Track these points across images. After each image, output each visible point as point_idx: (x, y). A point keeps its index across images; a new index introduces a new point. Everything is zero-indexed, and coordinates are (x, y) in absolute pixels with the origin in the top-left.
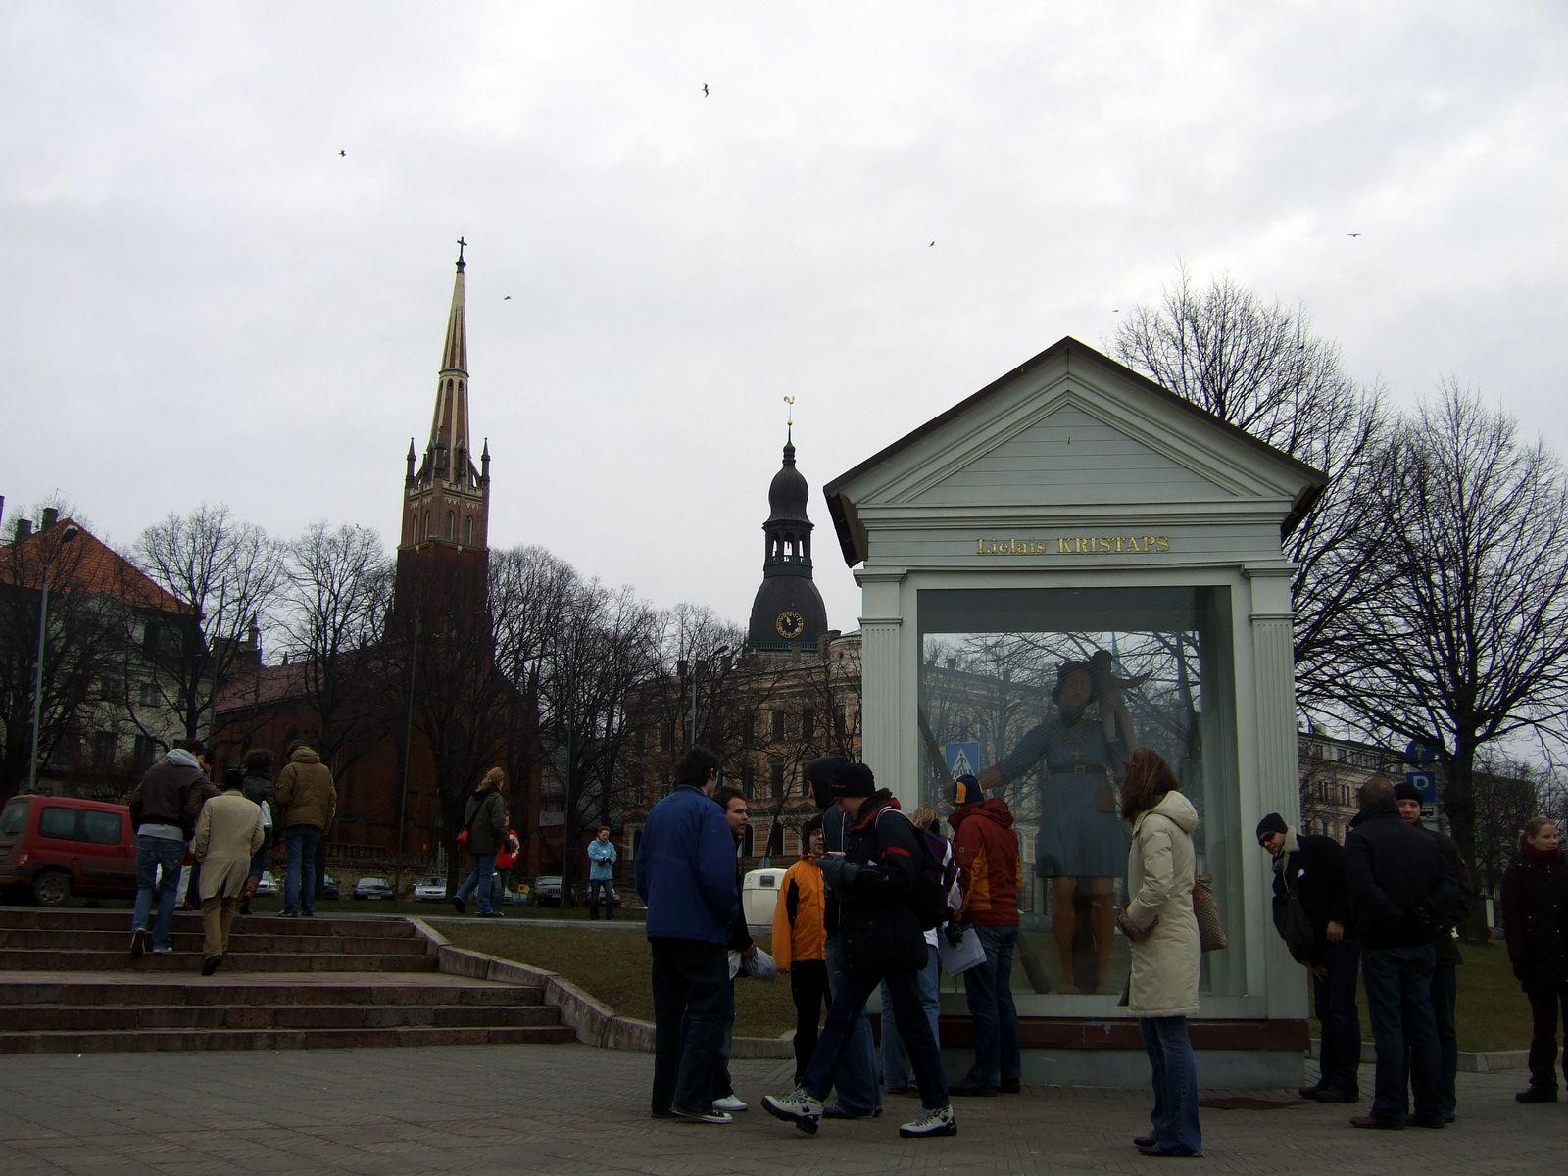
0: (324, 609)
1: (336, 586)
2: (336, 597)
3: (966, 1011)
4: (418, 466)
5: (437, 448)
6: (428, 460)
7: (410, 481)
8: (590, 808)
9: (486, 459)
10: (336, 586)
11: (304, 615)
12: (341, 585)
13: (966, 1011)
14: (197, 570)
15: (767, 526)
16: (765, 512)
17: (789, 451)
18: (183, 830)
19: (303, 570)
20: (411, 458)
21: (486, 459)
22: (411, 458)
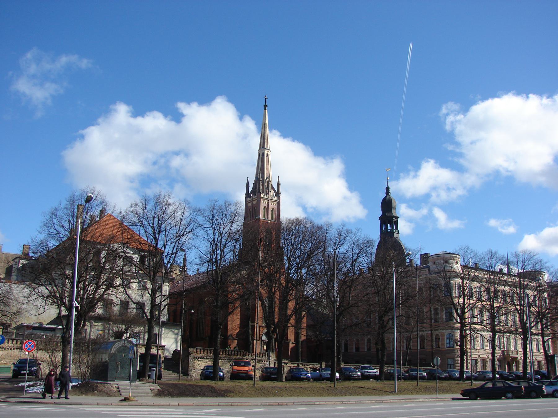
0: (216, 240)
1: (222, 229)
2: (221, 234)
3: (191, 350)
4: (251, 189)
5: (257, 180)
6: (255, 186)
7: (248, 195)
8: (462, 301)
9: (278, 184)
10: (222, 229)
11: (208, 244)
12: (224, 229)
13: (191, 350)
14: (156, 223)
15: (381, 218)
16: (379, 213)
17: (388, 189)
18: (218, 95)
19: (205, 222)
20: (248, 186)
21: (278, 184)
22: (248, 186)
